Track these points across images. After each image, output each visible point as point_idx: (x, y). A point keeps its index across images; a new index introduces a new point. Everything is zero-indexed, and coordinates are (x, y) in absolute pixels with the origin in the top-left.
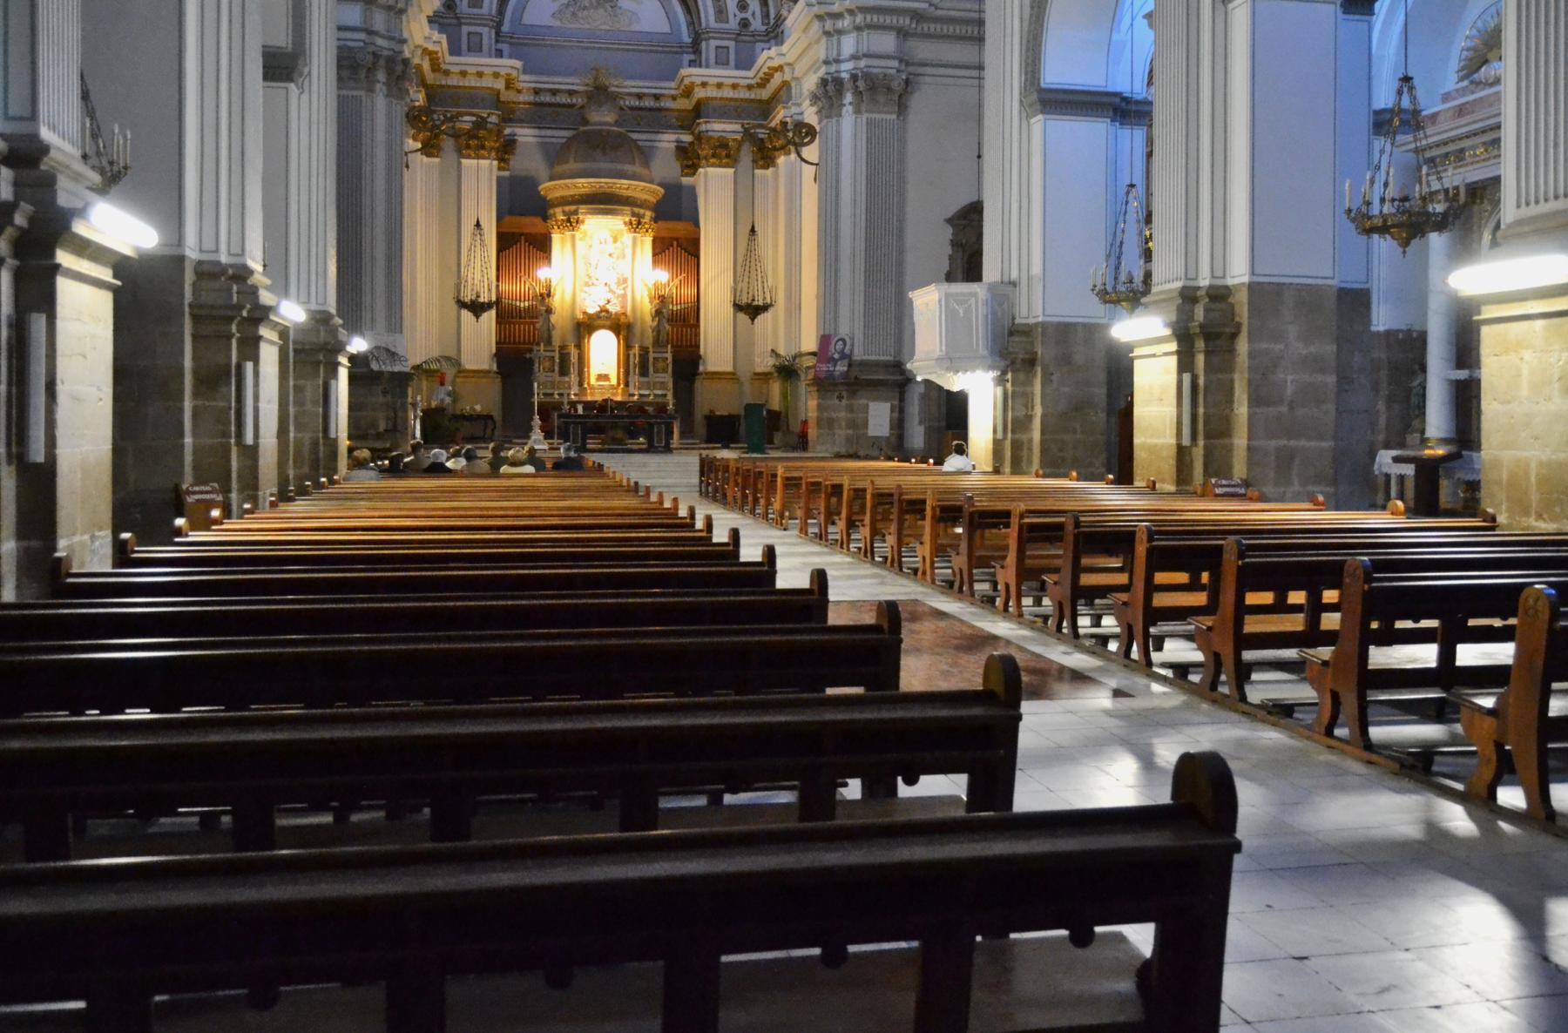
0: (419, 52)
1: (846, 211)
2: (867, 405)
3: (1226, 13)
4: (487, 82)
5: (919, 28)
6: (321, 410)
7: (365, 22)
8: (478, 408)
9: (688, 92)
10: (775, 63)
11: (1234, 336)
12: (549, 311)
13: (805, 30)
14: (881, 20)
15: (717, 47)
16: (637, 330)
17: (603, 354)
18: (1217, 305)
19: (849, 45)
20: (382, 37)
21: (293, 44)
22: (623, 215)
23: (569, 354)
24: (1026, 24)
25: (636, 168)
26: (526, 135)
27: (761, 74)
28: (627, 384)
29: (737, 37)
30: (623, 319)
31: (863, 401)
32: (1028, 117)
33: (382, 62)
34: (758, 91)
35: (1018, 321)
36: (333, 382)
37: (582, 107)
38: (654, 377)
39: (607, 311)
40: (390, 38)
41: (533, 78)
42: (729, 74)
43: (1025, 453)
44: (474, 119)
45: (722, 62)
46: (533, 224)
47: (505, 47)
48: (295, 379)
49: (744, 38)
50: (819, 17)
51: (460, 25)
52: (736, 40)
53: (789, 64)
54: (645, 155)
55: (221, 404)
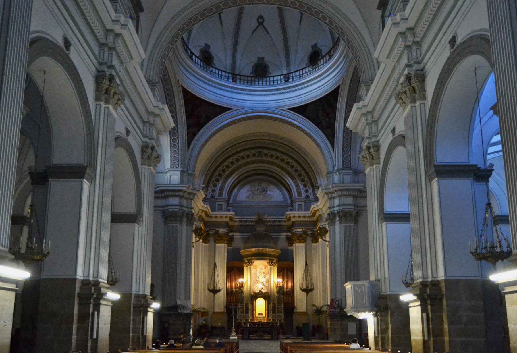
2: (347, 324)
3: (431, 184)
6: (141, 326)
7: (180, 203)
8: (219, 324)
9: (289, 219)
10: (316, 209)
11: (442, 299)
12: (242, 292)
14: (352, 193)
15: (298, 205)
17: (260, 305)
18: (435, 288)
19: (337, 202)
25: (271, 244)
26: (237, 235)
27: (312, 213)
28: (268, 316)
29: (305, 201)
33: (185, 214)
34: (312, 218)
35: (382, 294)
36: (146, 317)
37: (254, 225)
39: (261, 292)
41: (239, 217)
42: (302, 213)
43: (386, 341)
45: (300, 209)
46: (237, 264)
47: (231, 208)
49: (308, 201)
50: (326, 193)
52: (305, 202)
54: (275, 241)
55: (86, 325)
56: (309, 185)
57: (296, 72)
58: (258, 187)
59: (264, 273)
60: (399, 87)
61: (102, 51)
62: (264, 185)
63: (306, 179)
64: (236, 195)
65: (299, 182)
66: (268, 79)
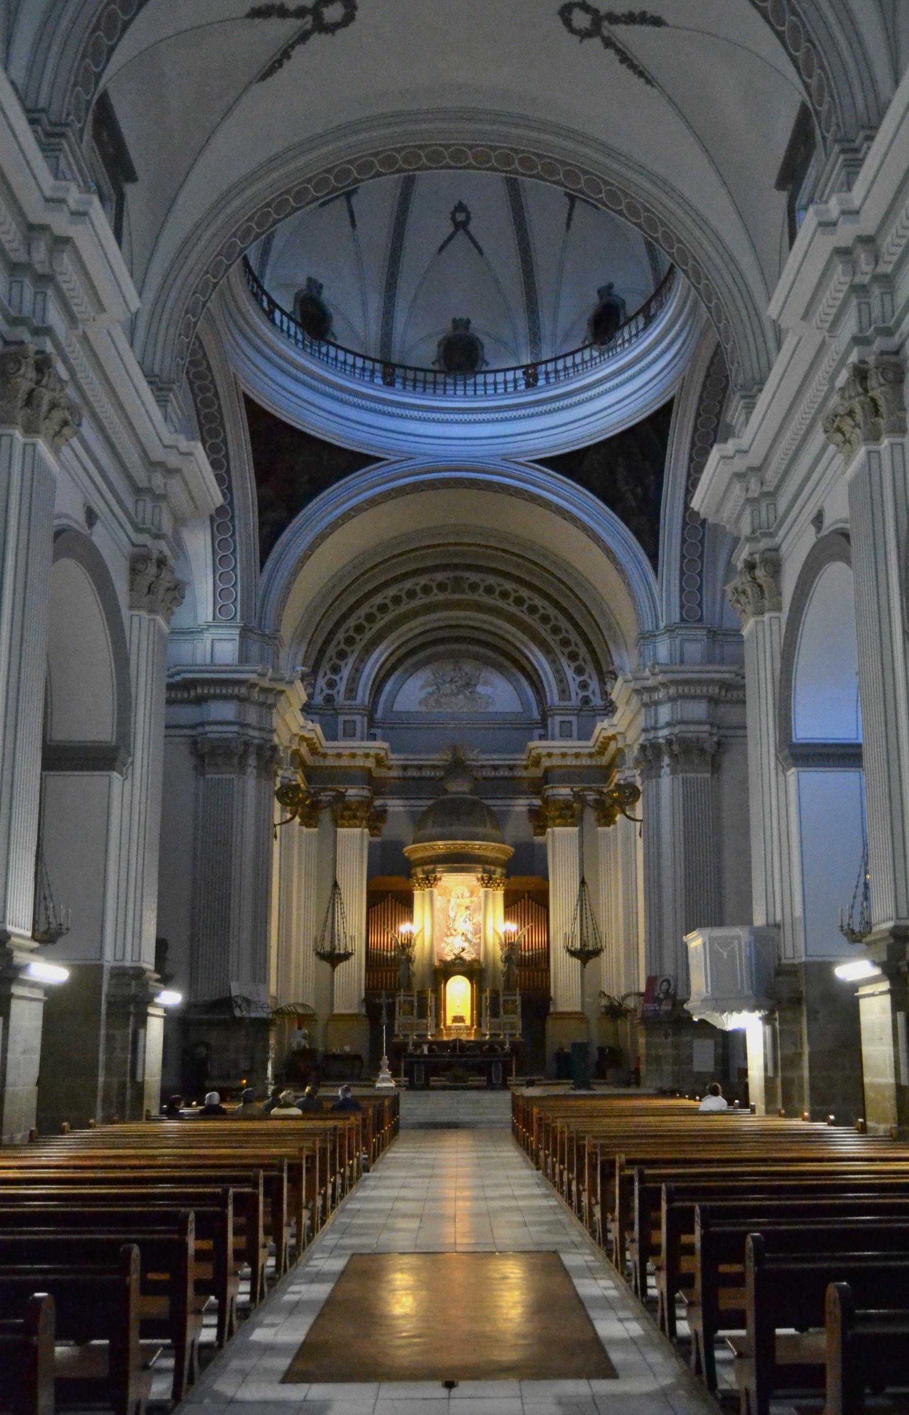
0: (297, 739)
1: (667, 863)
4: (359, 762)
5: (729, 696)
6: (129, 1056)
8: (347, 1049)
9: (537, 762)
10: (609, 733)
12: (409, 960)
13: (628, 702)
16: (489, 974)
19: (665, 713)
20: (254, 728)
21: (117, 739)
22: (475, 872)
23: (426, 998)
24: (777, 685)
25: (488, 830)
26: (395, 805)
27: (598, 744)
28: (480, 1025)
30: (476, 965)
31: (689, 1038)
32: (784, 771)
34: (598, 758)
35: (784, 961)
36: (142, 1031)
38: (504, 1018)
39: (461, 958)
40: (260, 729)
42: (572, 745)
44: (333, 793)
46: (394, 882)
48: (107, 1028)
50: (637, 691)
51: (338, 714)
53: (619, 733)
54: (498, 820)
56: (590, 669)
57: (556, 359)
58: (452, 674)
59: (467, 908)
60: (835, 399)
61: (16, 288)
62: (468, 667)
63: (583, 651)
64: (393, 697)
65: (564, 662)
66: (480, 379)
